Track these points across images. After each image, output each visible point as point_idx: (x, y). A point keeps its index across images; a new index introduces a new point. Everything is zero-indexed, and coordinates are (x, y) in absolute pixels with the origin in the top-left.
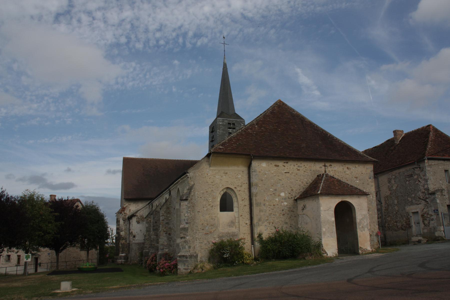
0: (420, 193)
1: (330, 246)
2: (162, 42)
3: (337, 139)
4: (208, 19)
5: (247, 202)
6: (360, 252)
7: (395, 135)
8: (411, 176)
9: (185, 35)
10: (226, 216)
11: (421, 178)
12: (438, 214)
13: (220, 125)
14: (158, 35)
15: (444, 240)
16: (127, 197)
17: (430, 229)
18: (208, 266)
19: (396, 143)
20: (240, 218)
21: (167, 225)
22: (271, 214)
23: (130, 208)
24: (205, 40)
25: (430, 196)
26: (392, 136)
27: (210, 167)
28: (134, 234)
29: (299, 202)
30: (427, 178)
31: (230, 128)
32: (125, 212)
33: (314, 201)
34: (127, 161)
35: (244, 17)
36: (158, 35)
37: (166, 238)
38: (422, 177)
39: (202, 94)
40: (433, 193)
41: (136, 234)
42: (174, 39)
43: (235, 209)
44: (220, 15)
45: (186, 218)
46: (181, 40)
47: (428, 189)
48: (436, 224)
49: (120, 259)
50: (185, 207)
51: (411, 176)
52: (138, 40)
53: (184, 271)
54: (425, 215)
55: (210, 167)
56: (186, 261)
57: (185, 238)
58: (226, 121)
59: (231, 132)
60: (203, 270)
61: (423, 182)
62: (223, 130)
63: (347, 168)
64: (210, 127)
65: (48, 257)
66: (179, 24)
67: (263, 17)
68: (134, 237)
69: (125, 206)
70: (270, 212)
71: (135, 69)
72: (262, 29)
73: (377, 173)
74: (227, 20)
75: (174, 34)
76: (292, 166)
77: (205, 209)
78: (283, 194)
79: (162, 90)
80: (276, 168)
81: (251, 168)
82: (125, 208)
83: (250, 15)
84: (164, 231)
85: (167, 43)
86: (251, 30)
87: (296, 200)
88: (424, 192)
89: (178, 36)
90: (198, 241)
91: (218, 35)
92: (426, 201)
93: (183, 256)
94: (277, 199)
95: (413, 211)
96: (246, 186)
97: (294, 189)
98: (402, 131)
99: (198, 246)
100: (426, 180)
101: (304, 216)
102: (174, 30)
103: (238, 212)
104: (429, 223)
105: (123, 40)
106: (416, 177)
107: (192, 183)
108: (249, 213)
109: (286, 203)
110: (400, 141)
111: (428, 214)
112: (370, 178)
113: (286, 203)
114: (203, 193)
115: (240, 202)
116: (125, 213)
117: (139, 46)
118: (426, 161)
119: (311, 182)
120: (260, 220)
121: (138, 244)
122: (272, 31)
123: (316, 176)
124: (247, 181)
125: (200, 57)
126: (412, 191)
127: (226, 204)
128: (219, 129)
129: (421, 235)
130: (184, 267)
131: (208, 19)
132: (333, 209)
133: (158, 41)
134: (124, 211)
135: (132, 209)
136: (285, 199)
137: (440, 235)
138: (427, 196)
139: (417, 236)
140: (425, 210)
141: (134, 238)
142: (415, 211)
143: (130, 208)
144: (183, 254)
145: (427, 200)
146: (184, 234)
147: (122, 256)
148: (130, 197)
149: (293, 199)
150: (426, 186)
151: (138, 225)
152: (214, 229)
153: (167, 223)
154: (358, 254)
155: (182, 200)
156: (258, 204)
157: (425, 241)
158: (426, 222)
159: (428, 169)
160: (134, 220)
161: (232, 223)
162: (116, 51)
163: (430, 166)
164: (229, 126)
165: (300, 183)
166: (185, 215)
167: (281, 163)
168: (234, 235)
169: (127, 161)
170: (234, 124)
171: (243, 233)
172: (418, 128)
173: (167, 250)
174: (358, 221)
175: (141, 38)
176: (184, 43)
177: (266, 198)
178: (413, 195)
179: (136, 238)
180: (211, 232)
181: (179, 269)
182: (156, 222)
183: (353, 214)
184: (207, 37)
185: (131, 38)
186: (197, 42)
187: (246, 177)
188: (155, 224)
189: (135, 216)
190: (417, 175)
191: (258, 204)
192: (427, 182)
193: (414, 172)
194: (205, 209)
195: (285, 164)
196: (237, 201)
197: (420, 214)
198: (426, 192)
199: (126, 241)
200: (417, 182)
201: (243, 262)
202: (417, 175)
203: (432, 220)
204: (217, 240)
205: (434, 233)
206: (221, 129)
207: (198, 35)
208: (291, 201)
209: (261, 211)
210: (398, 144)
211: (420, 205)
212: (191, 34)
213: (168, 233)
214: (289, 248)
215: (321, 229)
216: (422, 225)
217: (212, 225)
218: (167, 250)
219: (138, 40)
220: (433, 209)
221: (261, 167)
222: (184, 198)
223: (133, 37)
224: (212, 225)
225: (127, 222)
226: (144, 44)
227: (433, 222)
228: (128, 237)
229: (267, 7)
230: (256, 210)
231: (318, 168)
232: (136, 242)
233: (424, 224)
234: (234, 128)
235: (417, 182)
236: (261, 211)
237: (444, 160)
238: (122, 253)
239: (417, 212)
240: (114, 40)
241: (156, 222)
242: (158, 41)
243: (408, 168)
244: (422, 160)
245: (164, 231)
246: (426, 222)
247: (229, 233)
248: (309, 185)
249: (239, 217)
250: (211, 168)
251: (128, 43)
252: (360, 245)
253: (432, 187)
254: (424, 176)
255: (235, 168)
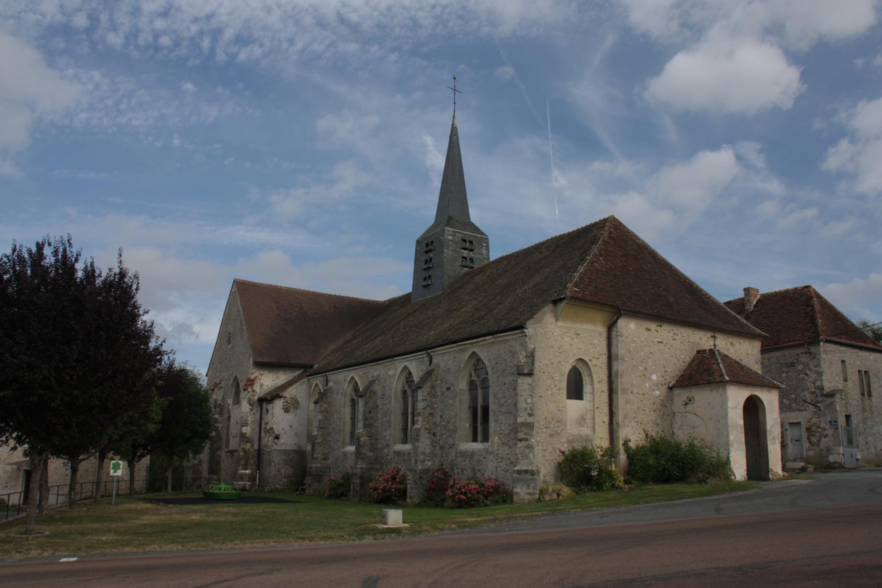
0: (806, 392)
1: (739, 468)
2: (165, 41)
3: (707, 294)
4: (269, 10)
5: (605, 387)
6: (770, 476)
7: (746, 295)
8: (792, 365)
9: (216, 34)
10: (574, 407)
11: (810, 370)
12: (837, 428)
13: (449, 240)
14: (159, 24)
15: (843, 467)
16: (259, 359)
17: (821, 450)
18: (566, 490)
19: (747, 308)
20: (596, 411)
21: (430, 418)
22: (639, 408)
23: (262, 381)
24: (258, 52)
25: (825, 399)
26: (741, 295)
27: (557, 321)
28: (276, 432)
29: (676, 391)
30: (820, 370)
31: (465, 249)
32: (254, 388)
33: (715, 391)
34: (244, 291)
35: (342, 20)
36: (159, 24)
37: (428, 442)
38: (812, 367)
39: (232, 159)
40: (831, 395)
41: (282, 432)
42: (192, 39)
43: (587, 396)
44: (294, 8)
45: (528, 407)
46: (206, 43)
47: (822, 388)
48: (831, 444)
49: (241, 480)
50: (526, 387)
51: (792, 365)
52: (114, 28)
53: (527, 496)
54: (814, 428)
55: (557, 321)
56: (530, 480)
57: (527, 440)
58: (459, 235)
59: (465, 255)
60: (558, 495)
61: (814, 376)
62: (453, 251)
63: (731, 344)
64: (418, 242)
65: (64, 470)
66: (208, 9)
67: (380, 26)
68: (277, 437)
69: (252, 377)
70: (638, 405)
71: (97, 86)
72: (374, 48)
73: (763, 351)
74: (308, 20)
75: (194, 29)
76: (667, 333)
77: (549, 393)
78: (654, 377)
79: (150, 139)
80: (646, 333)
81: (615, 329)
82: (253, 381)
83: (354, 18)
84: (426, 429)
85: (177, 44)
86: (353, 47)
87: (671, 388)
88: (814, 392)
89: (201, 34)
90: (540, 448)
91: (285, 45)
92: (816, 407)
93: (526, 472)
94: (647, 385)
95: (791, 421)
96: (604, 359)
97: (669, 370)
98: (757, 291)
99: (540, 455)
100: (820, 374)
101: (688, 415)
102: (196, 20)
103: (594, 401)
104: (819, 441)
105: (81, 21)
106: (800, 367)
107: (532, 346)
108: (607, 405)
109: (658, 393)
110: (755, 306)
111: (818, 427)
112: (757, 363)
113: (658, 393)
114: (547, 365)
115: (597, 385)
116: (253, 391)
117: (115, 40)
118: (822, 344)
119: (689, 360)
120: (626, 417)
121: (285, 452)
122: (393, 57)
123: (695, 353)
124: (605, 351)
125: (241, 85)
126: (791, 389)
127: (575, 390)
128: (447, 248)
129: (802, 459)
130: (528, 491)
131: (269, 10)
132: (741, 406)
133: (156, 37)
134: (252, 385)
135: (266, 384)
136: (657, 385)
137: (838, 460)
138: (820, 399)
139: (795, 460)
140: (813, 420)
141: (276, 441)
142: (796, 421)
143: (262, 381)
144: (525, 468)
145: (819, 405)
146: (525, 434)
147: (245, 474)
148: (265, 360)
149: (666, 386)
150: (818, 383)
151: (286, 415)
152: (561, 428)
153: (430, 414)
154: (767, 479)
155: (521, 374)
156: (625, 391)
157: (811, 468)
158: (814, 440)
159: (823, 356)
160: (278, 404)
161: (582, 420)
162: (60, 43)
163: (825, 352)
164: (464, 245)
165: (676, 361)
166: (526, 400)
167: (653, 326)
168: (588, 440)
169: (244, 291)
170: (471, 242)
171: (601, 441)
172: (785, 288)
173: (430, 463)
174: (768, 428)
175: (122, 24)
176: (212, 50)
177: (634, 382)
178: (793, 396)
179: (282, 441)
180: (557, 433)
181: (517, 493)
182: (370, 412)
183: (761, 417)
184: (261, 45)
185: (98, 20)
186: (239, 52)
187: (604, 343)
188: (368, 416)
189: (281, 397)
190: (803, 364)
191: (625, 391)
192: (821, 376)
193: (797, 359)
194: (549, 393)
195: (658, 328)
196: (592, 383)
197: (804, 425)
198: (817, 392)
199: (252, 446)
200: (801, 376)
201: (613, 485)
202: (803, 364)
203: (826, 436)
204: (565, 447)
205: (827, 457)
206: (451, 248)
207: (242, 40)
208: (664, 389)
209: (627, 402)
210: (753, 311)
211: (805, 412)
212: (229, 34)
213: (432, 432)
214: (670, 466)
215: (728, 436)
216: (806, 444)
217: (559, 421)
218: (430, 463)
219: (114, 28)
220: (829, 419)
221: (628, 327)
222: (526, 371)
223: (104, 18)
224: (559, 421)
225: (257, 409)
226: (127, 38)
227: (826, 440)
228: (256, 437)
229: (389, 9)
230: (621, 400)
231: (703, 340)
232: (280, 448)
233: (810, 442)
234: (471, 250)
235: (801, 376)
236: (627, 402)
237: (841, 344)
238: (246, 469)
239: (799, 424)
240: (59, 18)
241: (370, 412)
242: (156, 37)
243: (786, 352)
244: (815, 341)
245: (426, 429)
246: (814, 440)
247: (581, 436)
248: (686, 364)
249: (594, 410)
250: (558, 323)
251: (90, 30)
252: (771, 466)
253: (828, 386)
254: (816, 366)
255: (589, 327)
